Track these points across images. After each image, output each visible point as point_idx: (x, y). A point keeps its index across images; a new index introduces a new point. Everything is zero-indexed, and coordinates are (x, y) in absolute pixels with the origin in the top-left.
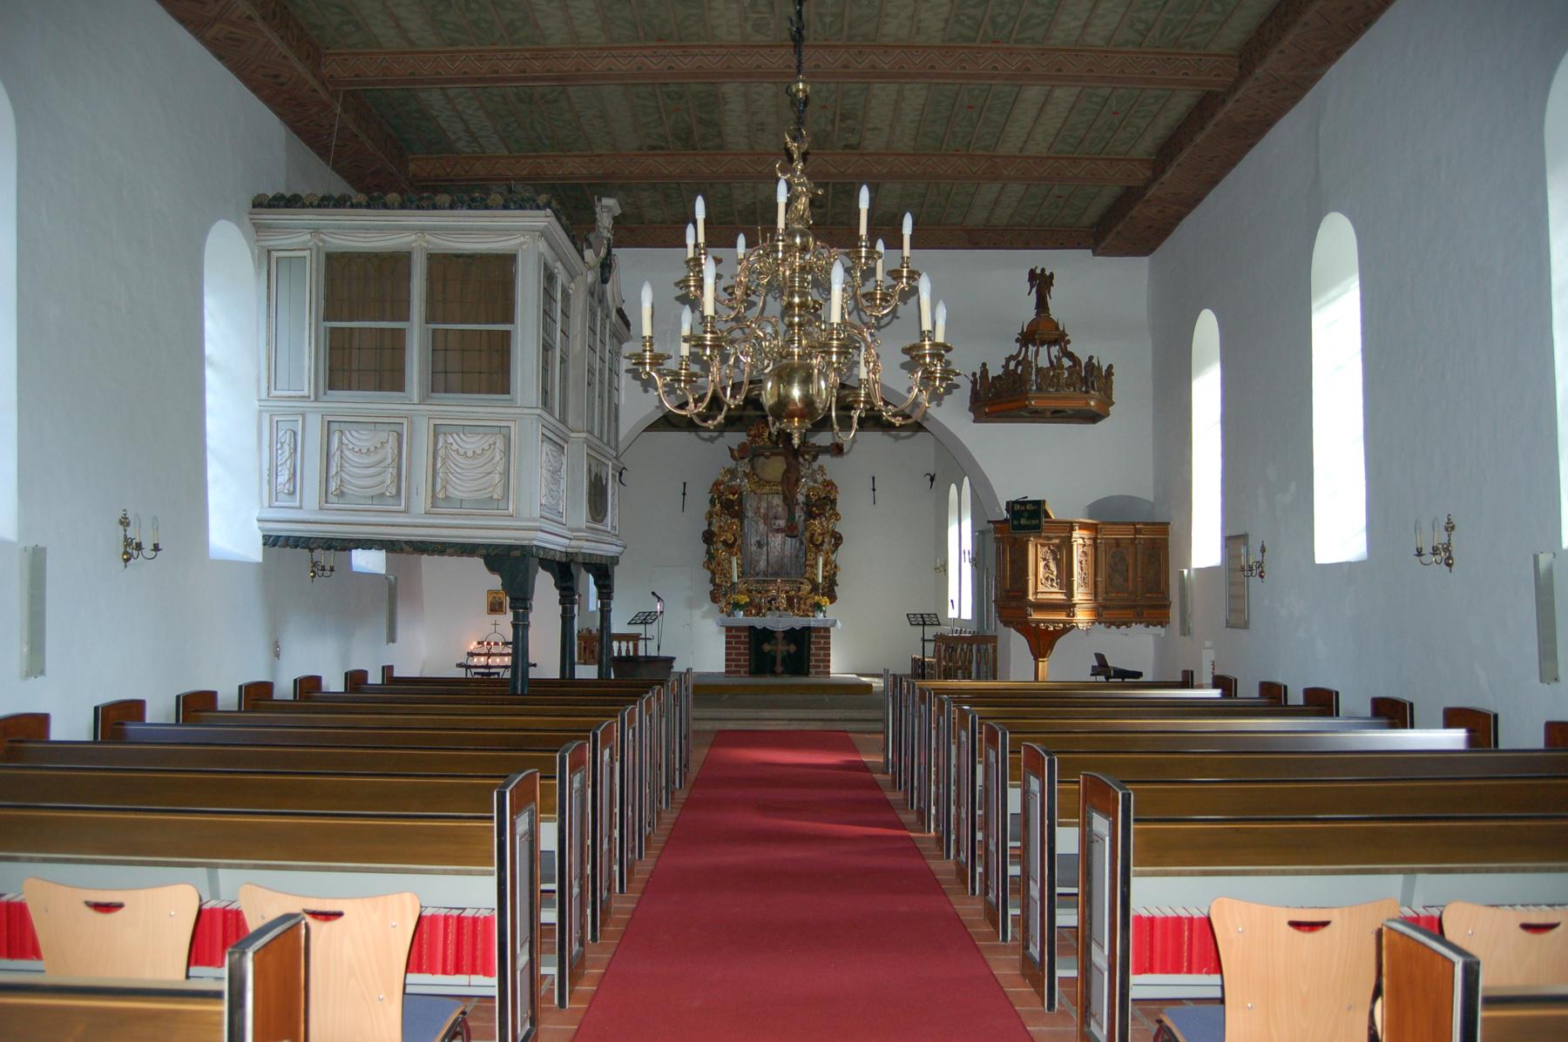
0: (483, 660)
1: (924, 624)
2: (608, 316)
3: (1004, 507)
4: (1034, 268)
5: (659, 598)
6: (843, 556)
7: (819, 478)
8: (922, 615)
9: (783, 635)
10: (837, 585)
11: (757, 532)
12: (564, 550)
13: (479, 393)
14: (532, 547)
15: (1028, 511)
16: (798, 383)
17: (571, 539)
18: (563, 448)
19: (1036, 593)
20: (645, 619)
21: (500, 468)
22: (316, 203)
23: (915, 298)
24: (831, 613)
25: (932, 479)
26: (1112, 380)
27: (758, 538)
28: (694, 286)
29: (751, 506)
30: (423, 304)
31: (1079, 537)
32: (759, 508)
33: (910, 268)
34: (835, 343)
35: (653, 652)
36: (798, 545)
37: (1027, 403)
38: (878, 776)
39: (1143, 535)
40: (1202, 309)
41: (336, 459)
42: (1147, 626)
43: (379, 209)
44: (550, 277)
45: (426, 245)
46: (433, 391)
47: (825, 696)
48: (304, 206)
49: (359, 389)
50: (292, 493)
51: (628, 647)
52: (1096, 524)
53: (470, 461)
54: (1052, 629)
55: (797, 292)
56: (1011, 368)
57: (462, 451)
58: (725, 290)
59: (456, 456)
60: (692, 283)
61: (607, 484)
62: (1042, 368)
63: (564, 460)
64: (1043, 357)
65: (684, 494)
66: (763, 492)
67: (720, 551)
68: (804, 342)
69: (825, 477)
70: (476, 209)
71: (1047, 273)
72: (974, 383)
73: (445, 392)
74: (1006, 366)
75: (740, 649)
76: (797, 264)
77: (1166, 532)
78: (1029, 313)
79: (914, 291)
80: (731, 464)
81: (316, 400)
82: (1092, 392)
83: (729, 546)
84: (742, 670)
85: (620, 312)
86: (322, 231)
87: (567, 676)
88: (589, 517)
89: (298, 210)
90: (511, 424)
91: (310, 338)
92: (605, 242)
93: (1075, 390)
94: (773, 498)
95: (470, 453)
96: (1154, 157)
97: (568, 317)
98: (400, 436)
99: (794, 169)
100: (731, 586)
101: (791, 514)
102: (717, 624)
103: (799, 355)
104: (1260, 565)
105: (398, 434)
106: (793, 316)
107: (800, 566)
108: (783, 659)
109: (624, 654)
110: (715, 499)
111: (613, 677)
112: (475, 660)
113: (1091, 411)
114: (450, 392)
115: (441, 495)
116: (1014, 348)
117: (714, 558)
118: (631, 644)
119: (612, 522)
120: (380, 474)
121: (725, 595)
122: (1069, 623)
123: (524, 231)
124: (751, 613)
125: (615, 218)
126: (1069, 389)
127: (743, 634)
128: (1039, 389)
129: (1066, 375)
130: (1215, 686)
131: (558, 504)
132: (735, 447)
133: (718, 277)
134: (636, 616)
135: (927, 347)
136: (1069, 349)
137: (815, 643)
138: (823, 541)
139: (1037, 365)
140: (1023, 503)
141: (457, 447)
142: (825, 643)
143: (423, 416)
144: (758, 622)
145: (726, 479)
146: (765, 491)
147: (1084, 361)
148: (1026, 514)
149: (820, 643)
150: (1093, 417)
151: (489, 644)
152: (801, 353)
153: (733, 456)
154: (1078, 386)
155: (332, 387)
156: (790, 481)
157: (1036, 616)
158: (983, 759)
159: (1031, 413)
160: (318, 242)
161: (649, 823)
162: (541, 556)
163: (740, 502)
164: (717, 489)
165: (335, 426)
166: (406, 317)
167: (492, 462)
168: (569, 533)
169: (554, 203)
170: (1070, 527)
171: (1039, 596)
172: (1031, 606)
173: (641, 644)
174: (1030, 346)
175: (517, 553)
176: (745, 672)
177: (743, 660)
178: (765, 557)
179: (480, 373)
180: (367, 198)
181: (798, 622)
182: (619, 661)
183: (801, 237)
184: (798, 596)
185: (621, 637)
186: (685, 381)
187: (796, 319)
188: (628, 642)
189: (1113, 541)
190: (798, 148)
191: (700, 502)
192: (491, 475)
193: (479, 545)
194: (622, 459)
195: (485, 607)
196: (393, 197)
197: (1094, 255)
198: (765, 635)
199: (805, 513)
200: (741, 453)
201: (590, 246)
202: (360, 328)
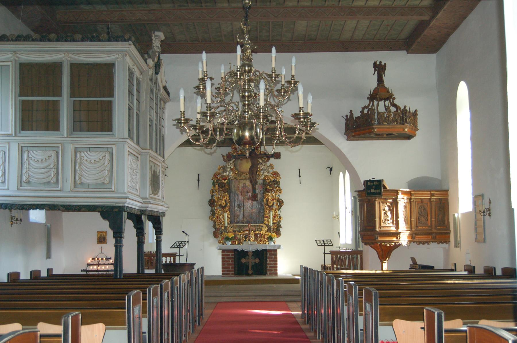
0: (95, 267)
1: (325, 245)
2: (159, 90)
3: (363, 183)
4: (376, 61)
5: (186, 234)
6: (284, 212)
7: (271, 171)
8: (323, 240)
9: (252, 254)
10: (281, 227)
11: (238, 200)
12: (139, 208)
13: (97, 131)
14: (124, 206)
15: (375, 185)
16: (248, 130)
17: (142, 203)
18: (138, 158)
19: (380, 227)
20: (179, 245)
21: (108, 168)
22: (14, 39)
23: (296, 92)
24: (278, 241)
25: (331, 170)
26: (417, 117)
27: (238, 203)
28: (202, 88)
29: (234, 186)
30: (69, 88)
31: (402, 200)
32: (238, 187)
33: (295, 80)
34: (262, 114)
35: (183, 261)
36: (260, 206)
37: (373, 130)
38: (308, 334)
39: (435, 196)
40: (461, 81)
41: (26, 165)
42: (439, 244)
43: (46, 41)
44: (131, 74)
45: (69, 59)
46: (74, 131)
47: (274, 285)
48: (8, 40)
49: (37, 130)
50: (3, 182)
51: (170, 260)
52: (411, 192)
53: (93, 165)
54: (389, 246)
55: (247, 91)
56: (365, 113)
57: (89, 160)
58: (216, 88)
59: (85, 162)
60: (201, 87)
61: (159, 175)
62: (380, 112)
63: (139, 164)
64: (381, 107)
65: (198, 180)
66: (241, 178)
67: (218, 211)
68: (250, 112)
69: (273, 170)
70: (94, 41)
71: (383, 63)
72: (347, 120)
73: (80, 131)
74: (362, 112)
75: (229, 261)
76: (247, 79)
77: (447, 195)
78: (373, 84)
79: (296, 89)
80: (223, 163)
81: (15, 136)
82: (406, 124)
83: (223, 207)
84: (231, 273)
85: (165, 88)
86: (18, 52)
87: (141, 272)
88: (151, 192)
89: (6, 42)
90: (113, 146)
91: (12, 105)
92: (157, 54)
93: (397, 123)
94: (246, 181)
95: (93, 161)
96: (433, 6)
97: (139, 92)
98: (58, 153)
99: (245, 37)
100: (224, 228)
101: (254, 189)
102: (217, 248)
103: (248, 118)
104: (489, 210)
105: (57, 152)
106: (245, 101)
107: (261, 217)
108: (253, 266)
109: (168, 262)
110: (215, 182)
111: (163, 272)
112: (91, 268)
113: (405, 134)
114: (82, 131)
115: (78, 182)
116: (367, 102)
117: (215, 214)
118: (172, 258)
119: (162, 194)
120: (48, 172)
121: (221, 234)
122: (397, 242)
123: (118, 52)
124: (235, 243)
125: (162, 41)
126: (394, 123)
127: (231, 254)
128: (379, 123)
129: (392, 116)
130: (465, 270)
131: (136, 185)
132: (225, 155)
133: (212, 85)
134: (174, 244)
135: (302, 114)
136: (395, 103)
137: (269, 258)
138: (273, 204)
139: (378, 111)
140: (372, 181)
141: (87, 158)
142: (275, 258)
143: (69, 143)
144: (239, 247)
145: (221, 172)
146: (242, 178)
147: (402, 108)
148: (374, 187)
149: (272, 258)
150: (409, 137)
151: (98, 259)
152: (249, 117)
153: (224, 160)
154: (399, 121)
155: (23, 129)
156: (253, 172)
157: (381, 239)
158: (347, 303)
159: (376, 135)
160: (15, 58)
161: (185, 335)
162: (128, 211)
163: (229, 184)
164: (216, 177)
165: (25, 149)
166: (60, 95)
167: (104, 165)
168: (142, 200)
169: (133, 39)
170: (396, 192)
171: (382, 229)
172: (377, 234)
173: (177, 258)
174: (375, 101)
175: (117, 210)
176: (232, 274)
177: (231, 268)
178: (242, 213)
179: (97, 121)
180: (40, 36)
181: (260, 246)
182: (166, 266)
183: (248, 67)
184: (260, 233)
185: (167, 255)
186: (199, 129)
187: (247, 102)
188: (170, 257)
189: (420, 200)
190: (246, 28)
191: (207, 184)
192: (103, 172)
193: (98, 206)
194: (166, 162)
195: (96, 240)
196: (53, 36)
197: (408, 54)
198: (243, 254)
199: (263, 189)
200: (228, 158)
201: (149, 57)
202: (37, 100)
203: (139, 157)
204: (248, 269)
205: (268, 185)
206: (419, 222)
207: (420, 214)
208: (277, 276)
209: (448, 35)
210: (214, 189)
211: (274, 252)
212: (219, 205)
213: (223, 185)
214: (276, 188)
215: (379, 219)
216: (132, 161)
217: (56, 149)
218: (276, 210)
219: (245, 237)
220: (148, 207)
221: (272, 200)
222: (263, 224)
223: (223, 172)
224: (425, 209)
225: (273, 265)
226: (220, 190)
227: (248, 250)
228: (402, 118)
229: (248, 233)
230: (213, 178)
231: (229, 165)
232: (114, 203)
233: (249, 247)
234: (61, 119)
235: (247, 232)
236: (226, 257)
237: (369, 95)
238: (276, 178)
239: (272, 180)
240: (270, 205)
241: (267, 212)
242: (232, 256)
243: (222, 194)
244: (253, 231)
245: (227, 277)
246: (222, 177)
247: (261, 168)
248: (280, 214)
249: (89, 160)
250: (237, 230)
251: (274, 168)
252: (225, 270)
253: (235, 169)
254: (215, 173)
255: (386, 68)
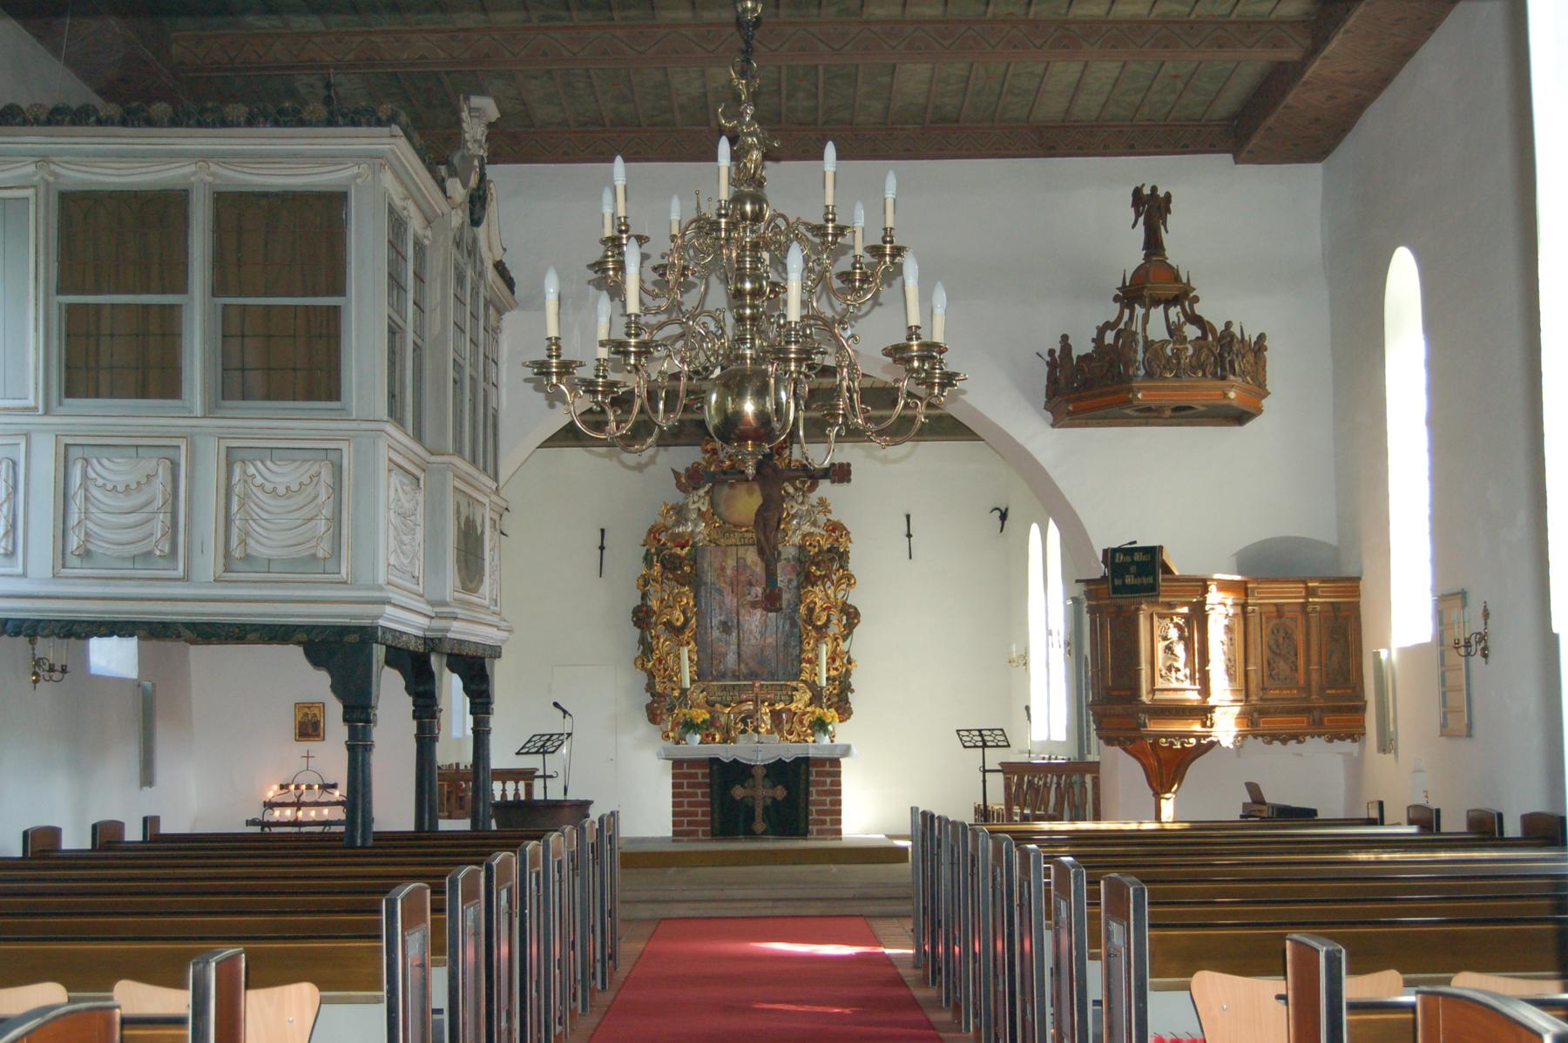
0: (288, 813)
1: (985, 746)
2: (481, 275)
3: (1100, 556)
4: (1139, 185)
5: (565, 712)
6: (861, 645)
7: (822, 519)
8: (980, 731)
9: (765, 771)
10: (852, 691)
11: (720, 608)
12: (420, 634)
13: (294, 400)
14: (377, 628)
15: (1137, 564)
16: (752, 395)
17: (432, 618)
18: (418, 480)
19: (1153, 691)
20: (543, 746)
21: (327, 512)
22: (43, 117)
23: (899, 279)
24: (843, 732)
25: (1003, 516)
26: (1265, 357)
27: (722, 618)
28: (613, 269)
29: (711, 565)
30: (209, 267)
31: (1220, 608)
32: (723, 569)
33: (895, 244)
34: (793, 347)
35: (555, 794)
36: (787, 627)
37: (1130, 396)
38: (935, 1017)
39: (1319, 597)
40: (1398, 246)
41: (78, 502)
42: (1330, 741)
43: (139, 126)
44: (397, 224)
45: (210, 179)
46: (223, 398)
47: (832, 866)
48: (25, 122)
49: (111, 396)
50: (10, 554)
51: (517, 790)
52: (1245, 583)
53: (282, 502)
54: (1179, 747)
55: (749, 276)
56: (1106, 342)
57: (269, 487)
58: (655, 269)
59: (259, 493)
60: (610, 266)
61: (483, 533)
62: (1153, 341)
63: (420, 497)
64: (1156, 324)
65: (602, 548)
66: (730, 542)
67: (662, 640)
68: (757, 342)
69: (829, 516)
70: (286, 125)
71: (1161, 193)
72: (1052, 365)
73: (243, 399)
74: (1099, 340)
75: (695, 795)
76: (748, 240)
77: (1356, 592)
78: (1132, 255)
79: (899, 270)
80: (677, 497)
81: (47, 413)
82: (1232, 377)
83: (676, 631)
84: (700, 829)
85: (500, 267)
86: (55, 159)
87: (426, 828)
88: (458, 584)
89: (17, 129)
90: (343, 445)
91: (36, 319)
92: (476, 163)
93: (1204, 374)
94: (747, 550)
95: (281, 490)
96: (1312, 18)
97: (422, 281)
98: (175, 465)
99: (742, 113)
100: (681, 694)
101: (771, 576)
102: (659, 754)
103: (751, 358)
104: (1482, 637)
105: (172, 462)
106: (744, 307)
107: (793, 660)
108: (766, 809)
109: (510, 797)
110: (652, 555)
111: (494, 827)
112: (277, 814)
113: (1229, 406)
114: (249, 399)
115: (237, 553)
116: (1112, 311)
117: (652, 651)
118: (522, 785)
119: (491, 591)
120: (147, 522)
121: (671, 710)
122: (1205, 737)
123: (358, 157)
124: (714, 739)
125: (490, 125)
126: (1195, 373)
127: (700, 772)
128: (1150, 375)
129: (1190, 351)
130: (1411, 822)
131: (412, 563)
132: (682, 471)
133: (644, 257)
134: (529, 742)
135: (915, 348)
136: (1197, 312)
137: (817, 783)
138: (828, 620)
139: (1145, 337)
140: (1129, 551)
141: (263, 481)
142: (833, 783)
143: (210, 434)
144: (725, 752)
145: (670, 522)
146: (733, 541)
147: (1220, 328)
148: (1133, 569)
149: (824, 783)
150: (1239, 417)
151: (297, 787)
152: (754, 356)
153: (679, 485)
154: (1209, 369)
155: (71, 391)
156: (768, 522)
157: (1154, 727)
158: (1051, 922)
159: (1140, 410)
160: (46, 176)
161: (560, 1019)
162: (389, 642)
163: (694, 559)
164: (655, 538)
165: (75, 453)
166: (183, 289)
167: (316, 502)
168: (429, 608)
169: (404, 118)
170: (1202, 585)
171: (1158, 696)
172: (1143, 712)
173: (538, 785)
174: (1137, 306)
175: (354, 638)
176: (704, 833)
177: (701, 813)
178: (734, 647)
179: (294, 369)
180: (121, 110)
181: (787, 749)
182: (504, 808)
183: (753, 203)
184: (790, 710)
185: (505, 775)
186: (602, 392)
187: (748, 311)
188: (517, 783)
189: (1273, 609)
190: (747, 85)
191: (628, 560)
192: (314, 522)
193: (298, 626)
194: (502, 493)
195: (290, 728)
196: (160, 108)
197: (1236, 163)
198: (736, 772)
199: (798, 574)
200: (692, 479)
201: (453, 173)
202: (112, 305)
203: (422, 477)
204: (753, 819)
205: (813, 563)
206: (1271, 676)
207: (1273, 652)
208: (841, 839)
209: (1359, 106)
210: (650, 575)
211: (831, 767)
212: (664, 624)
213: (677, 562)
214: (838, 570)
215: (1149, 666)
216: (400, 490)
217: (171, 453)
218: (836, 639)
219: (744, 721)
220: (448, 630)
221: (824, 609)
222: (797, 680)
223: (678, 523)
224: (1288, 636)
225: (828, 807)
226: (667, 578)
227: (751, 760)
228: (1220, 360)
229: (751, 707)
230: (645, 541)
231: (694, 502)
232: (345, 617)
233: (756, 751)
234: (185, 363)
235: (749, 706)
236: (685, 782)
237: (1118, 289)
238: (837, 540)
239: (825, 548)
240: (819, 623)
241: (809, 644)
242: (703, 778)
243: (673, 589)
244: (766, 704)
245: (688, 841)
246: (674, 537)
247: (793, 512)
248: (848, 652)
249: (269, 487)
250: (719, 699)
251: (830, 512)
252: (683, 821)
253: (713, 514)
254: (653, 527)
255: (1172, 206)
